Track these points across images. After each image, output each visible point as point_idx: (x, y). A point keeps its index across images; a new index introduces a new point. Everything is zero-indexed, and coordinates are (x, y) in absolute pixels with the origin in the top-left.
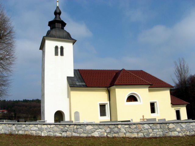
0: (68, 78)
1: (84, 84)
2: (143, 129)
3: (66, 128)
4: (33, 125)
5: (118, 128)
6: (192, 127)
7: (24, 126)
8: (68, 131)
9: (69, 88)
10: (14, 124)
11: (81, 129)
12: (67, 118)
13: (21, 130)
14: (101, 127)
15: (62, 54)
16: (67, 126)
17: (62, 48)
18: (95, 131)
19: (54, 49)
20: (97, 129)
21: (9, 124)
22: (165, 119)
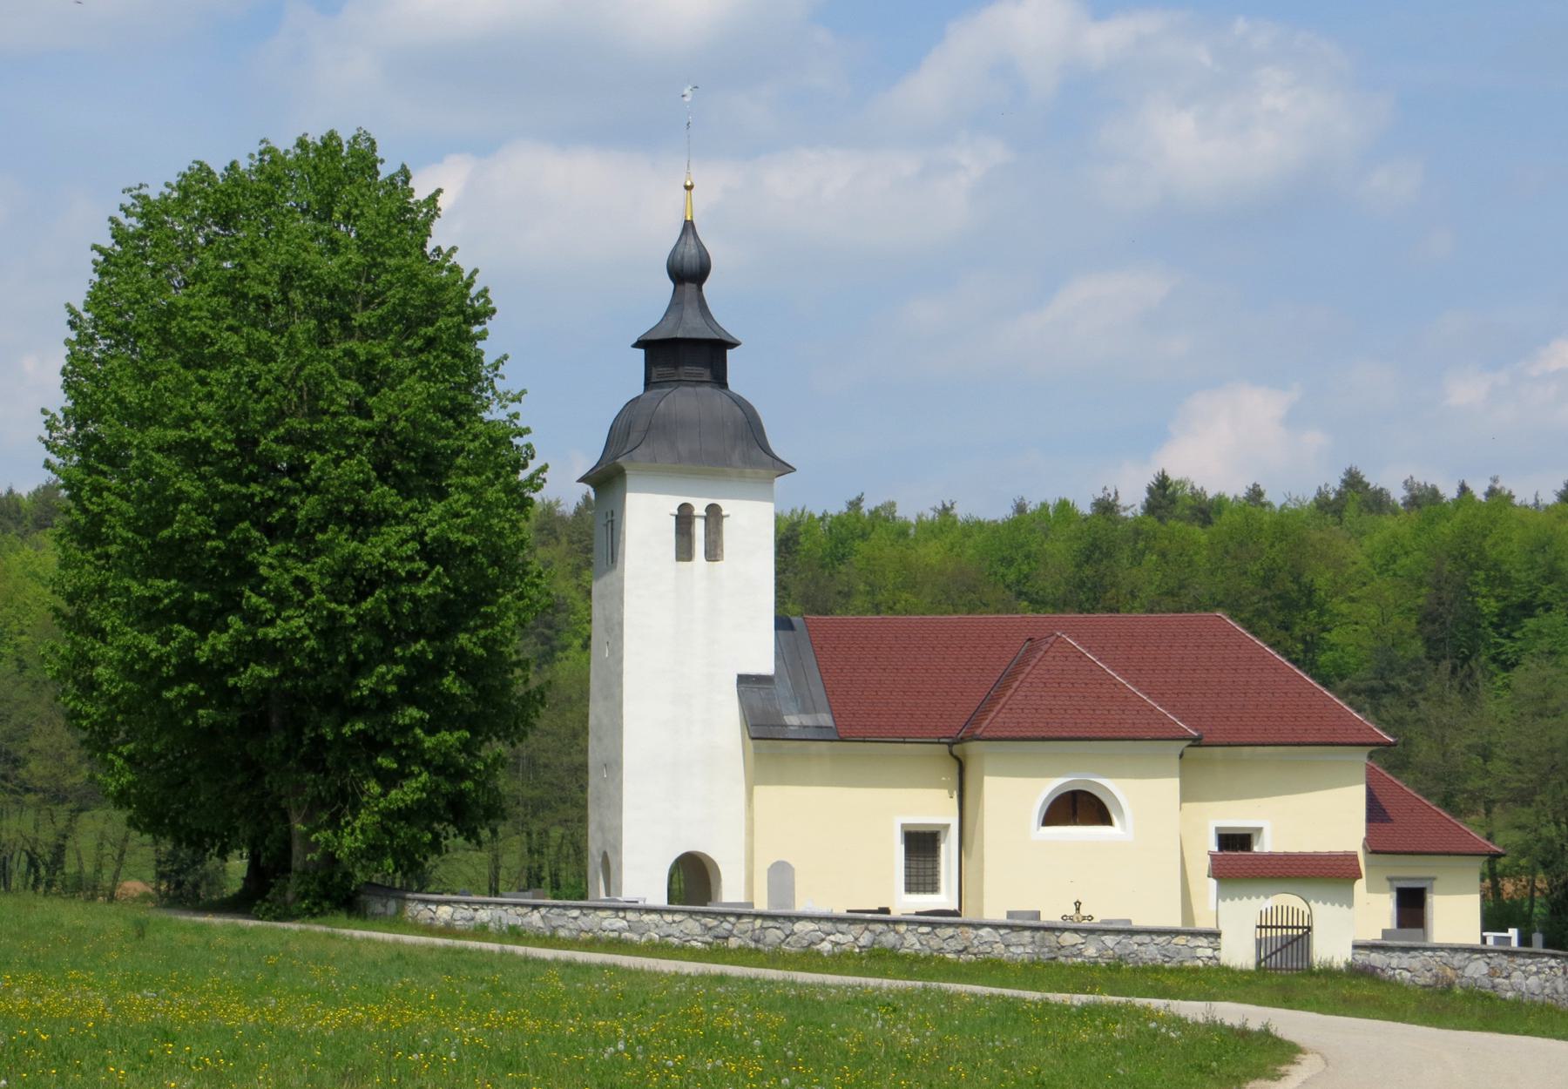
0: (743, 680)
1: (826, 719)
2: (976, 942)
3: (727, 926)
4: (609, 913)
5: (897, 933)
6: (1136, 947)
7: (576, 913)
8: (735, 936)
9: (750, 743)
10: (536, 907)
11: (778, 932)
12: (731, 891)
13: (563, 927)
14: (843, 927)
15: (713, 553)
16: (732, 919)
17: (714, 514)
18: (823, 940)
19: (671, 523)
20: (829, 934)
21: (516, 905)
22: (1129, 922)
